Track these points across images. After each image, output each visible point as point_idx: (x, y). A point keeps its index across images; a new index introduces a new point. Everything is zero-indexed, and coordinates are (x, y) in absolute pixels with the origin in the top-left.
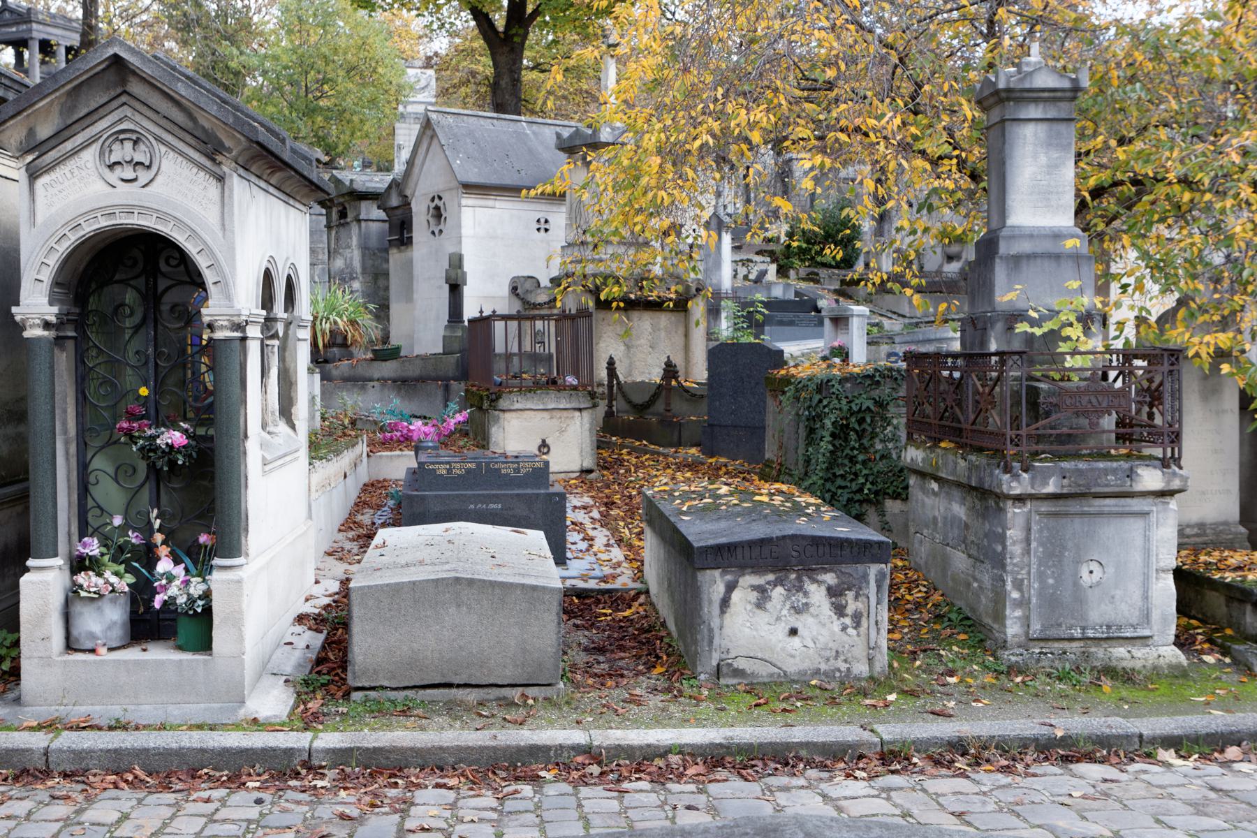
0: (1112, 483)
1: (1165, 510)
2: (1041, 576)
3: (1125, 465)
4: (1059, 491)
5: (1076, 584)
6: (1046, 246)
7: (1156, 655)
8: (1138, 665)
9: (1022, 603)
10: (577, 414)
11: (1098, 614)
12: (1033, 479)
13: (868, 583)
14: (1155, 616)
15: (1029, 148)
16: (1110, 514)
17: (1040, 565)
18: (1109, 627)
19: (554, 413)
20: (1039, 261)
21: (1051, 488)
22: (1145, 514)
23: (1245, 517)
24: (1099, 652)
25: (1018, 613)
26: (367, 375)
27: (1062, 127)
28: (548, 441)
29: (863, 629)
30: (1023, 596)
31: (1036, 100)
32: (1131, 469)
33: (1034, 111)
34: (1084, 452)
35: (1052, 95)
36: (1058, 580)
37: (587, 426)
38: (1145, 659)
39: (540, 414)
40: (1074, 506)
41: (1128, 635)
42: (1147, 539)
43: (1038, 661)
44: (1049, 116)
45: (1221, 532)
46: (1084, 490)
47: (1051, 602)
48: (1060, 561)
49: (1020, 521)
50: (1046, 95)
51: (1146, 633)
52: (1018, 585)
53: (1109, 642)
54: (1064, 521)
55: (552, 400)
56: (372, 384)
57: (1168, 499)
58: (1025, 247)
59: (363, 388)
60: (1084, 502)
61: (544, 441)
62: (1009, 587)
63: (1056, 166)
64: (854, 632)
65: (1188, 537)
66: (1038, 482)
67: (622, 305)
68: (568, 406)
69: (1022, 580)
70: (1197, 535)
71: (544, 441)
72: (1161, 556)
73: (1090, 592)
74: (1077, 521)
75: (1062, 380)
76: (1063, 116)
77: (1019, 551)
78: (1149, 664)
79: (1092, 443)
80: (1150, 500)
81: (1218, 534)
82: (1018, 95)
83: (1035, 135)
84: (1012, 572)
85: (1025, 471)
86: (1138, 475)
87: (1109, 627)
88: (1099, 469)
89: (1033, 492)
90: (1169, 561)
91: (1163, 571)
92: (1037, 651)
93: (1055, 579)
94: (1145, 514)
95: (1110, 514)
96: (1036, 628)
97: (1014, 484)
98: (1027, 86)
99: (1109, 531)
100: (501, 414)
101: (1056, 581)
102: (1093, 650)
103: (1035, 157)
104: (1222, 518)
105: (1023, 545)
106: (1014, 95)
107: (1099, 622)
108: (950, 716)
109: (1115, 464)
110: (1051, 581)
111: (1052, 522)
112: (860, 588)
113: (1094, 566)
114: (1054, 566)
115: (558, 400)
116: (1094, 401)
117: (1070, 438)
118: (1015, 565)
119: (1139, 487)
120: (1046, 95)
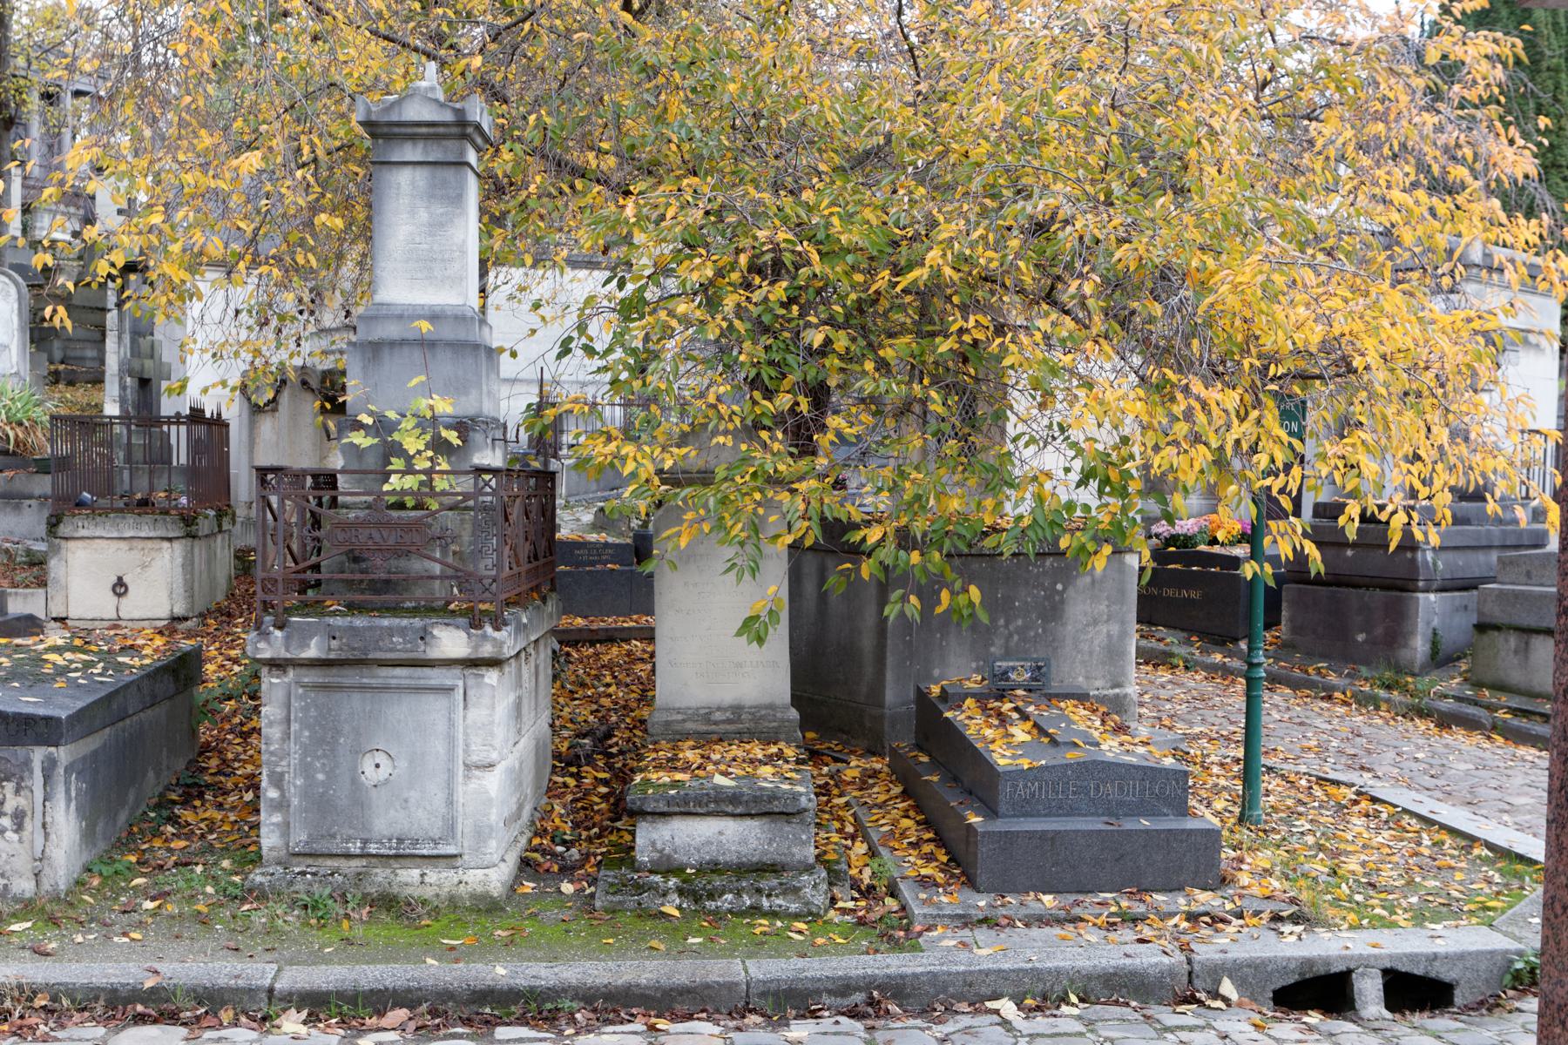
0: (399, 646)
1: (479, 685)
2: (306, 770)
3: (417, 622)
4: (323, 656)
5: (355, 781)
7: (456, 880)
8: (428, 893)
9: (281, 805)
10: (166, 545)
11: (385, 822)
12: (287, 638)
13: (32, 772)
15: (404, 201)
16: (399, 688)
17: (305, 754)
18: (400, 841)
19: (135, 543)
20: (406, 350)
21: (313, 651)
23: (797, 700)
24: (381, 875)
25: (277, 818)
26: (26, 491)
28: (126, 579)
29: (26, 834)
30: (283, 795)
31: (413, 138)
32: (425, 629)
33: (411, 152)
34: (408, 604)
35: (432, 130)
36: (330, 774)
37: (179, 560)
39: (115, 545)
40: (351, 677)
41: (425, 852)
42: (451, 723)
43: (291, 883)
44: (430, 159)
45: (762, 717)
46: (358, 655)
47: (320, 805)
48: (332, 750)
49: (279, 694)
50: (424, 130)
51: (451, 850)
52: (278, 781)
53: (402, 861)
54: (338, 696)
55: (129, 527)
56: (28, 502)
57: (483, 671)
58: (391, 331)
59: (17, 507)
61: (120, 579)
63: (442, 225)
64: (15, 837)
65: (716, 723)
66: (294, 643)
68: (152, 534)
69: (282, 774)
70: (728, 721)
71: (120, 579)
72: (473, 747)
73: (374, 792)
74: (356, 697)
78: (444, 892)
79: (419, 593)
80: (457, 671)
81: (756, 719)
82: (385, 130)
83: (413, 183)
85: (281, 628)
86: (434, 637)
88: (382, 628)
91: (477, 767)
92: (297, 870)
93: (326, 773)
94: (449, 690)
95: (399, 688)
96: (299, 837)
97: (261, 645)
98: (394, 118)
99: (400, 711)
100: (63, 543)
101: (328, 778)
103: (413, 212)
104: (766, 700)
105: (284, 727)
108: (48, 955)
109: (405, 622)
110: (320, 777)
111: (322, 698)
112: (22, 779)
114: (325, 756)
115: (138, 526)
117: (387, 585)
118: (272, 753)
119: (434, 653)
120: (424, 130)
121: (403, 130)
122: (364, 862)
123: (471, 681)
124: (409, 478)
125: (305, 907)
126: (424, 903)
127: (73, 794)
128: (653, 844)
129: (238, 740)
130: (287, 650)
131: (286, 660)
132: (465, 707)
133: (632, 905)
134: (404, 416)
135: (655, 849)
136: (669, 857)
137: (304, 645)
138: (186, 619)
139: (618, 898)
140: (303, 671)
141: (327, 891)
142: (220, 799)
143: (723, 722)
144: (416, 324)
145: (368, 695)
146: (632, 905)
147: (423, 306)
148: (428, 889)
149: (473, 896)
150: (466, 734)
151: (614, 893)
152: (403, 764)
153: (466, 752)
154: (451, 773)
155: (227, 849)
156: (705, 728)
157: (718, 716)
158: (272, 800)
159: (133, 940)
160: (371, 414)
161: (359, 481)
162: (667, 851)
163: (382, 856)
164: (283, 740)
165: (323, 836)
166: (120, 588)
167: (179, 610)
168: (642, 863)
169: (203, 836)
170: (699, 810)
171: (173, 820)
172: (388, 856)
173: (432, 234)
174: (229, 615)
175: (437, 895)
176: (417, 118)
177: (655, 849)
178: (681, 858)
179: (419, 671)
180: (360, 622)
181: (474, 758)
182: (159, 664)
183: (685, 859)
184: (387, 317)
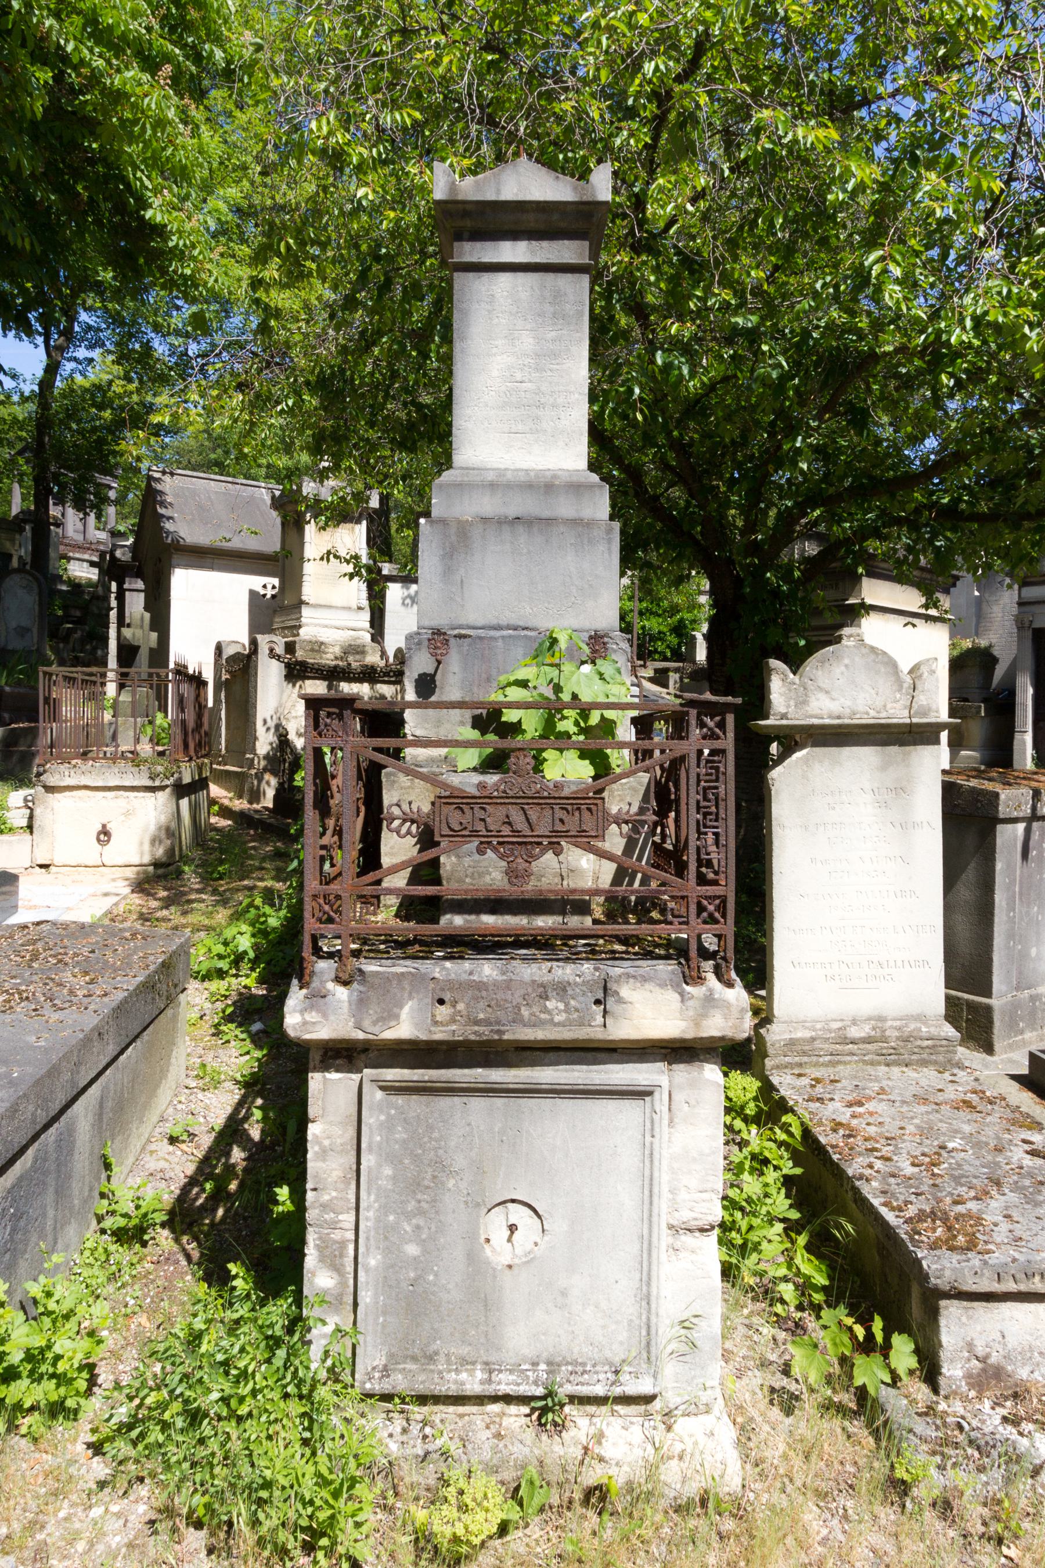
5: (473, 1258)
12: (361, 1004)
17: (385, 1209)
18: (553, 1366)
22: (641, 1094)
27: (563, 281)
28: (108, 827)
51: (645, 1387)
54: (444, 1102)
61: (104, 826)
63: (554, 355)
66: (373, 1011)
71: (104, 826)
75: (200, 784)
86: (621, 1001)
87: (553, 1366)
93: (422, 1243)
94: (641, 1094)
101: (425, 1252)
107: (529, 1352)
110: (412, 1250)
111: (416, 1104)
114: (421, 1212)
116: (518, 818)
128: (970, 1346)
137: (390, 1017)
154: (648, 1247)
157: (854, 1032)
162: (993, 1360)
166: (104, 834)
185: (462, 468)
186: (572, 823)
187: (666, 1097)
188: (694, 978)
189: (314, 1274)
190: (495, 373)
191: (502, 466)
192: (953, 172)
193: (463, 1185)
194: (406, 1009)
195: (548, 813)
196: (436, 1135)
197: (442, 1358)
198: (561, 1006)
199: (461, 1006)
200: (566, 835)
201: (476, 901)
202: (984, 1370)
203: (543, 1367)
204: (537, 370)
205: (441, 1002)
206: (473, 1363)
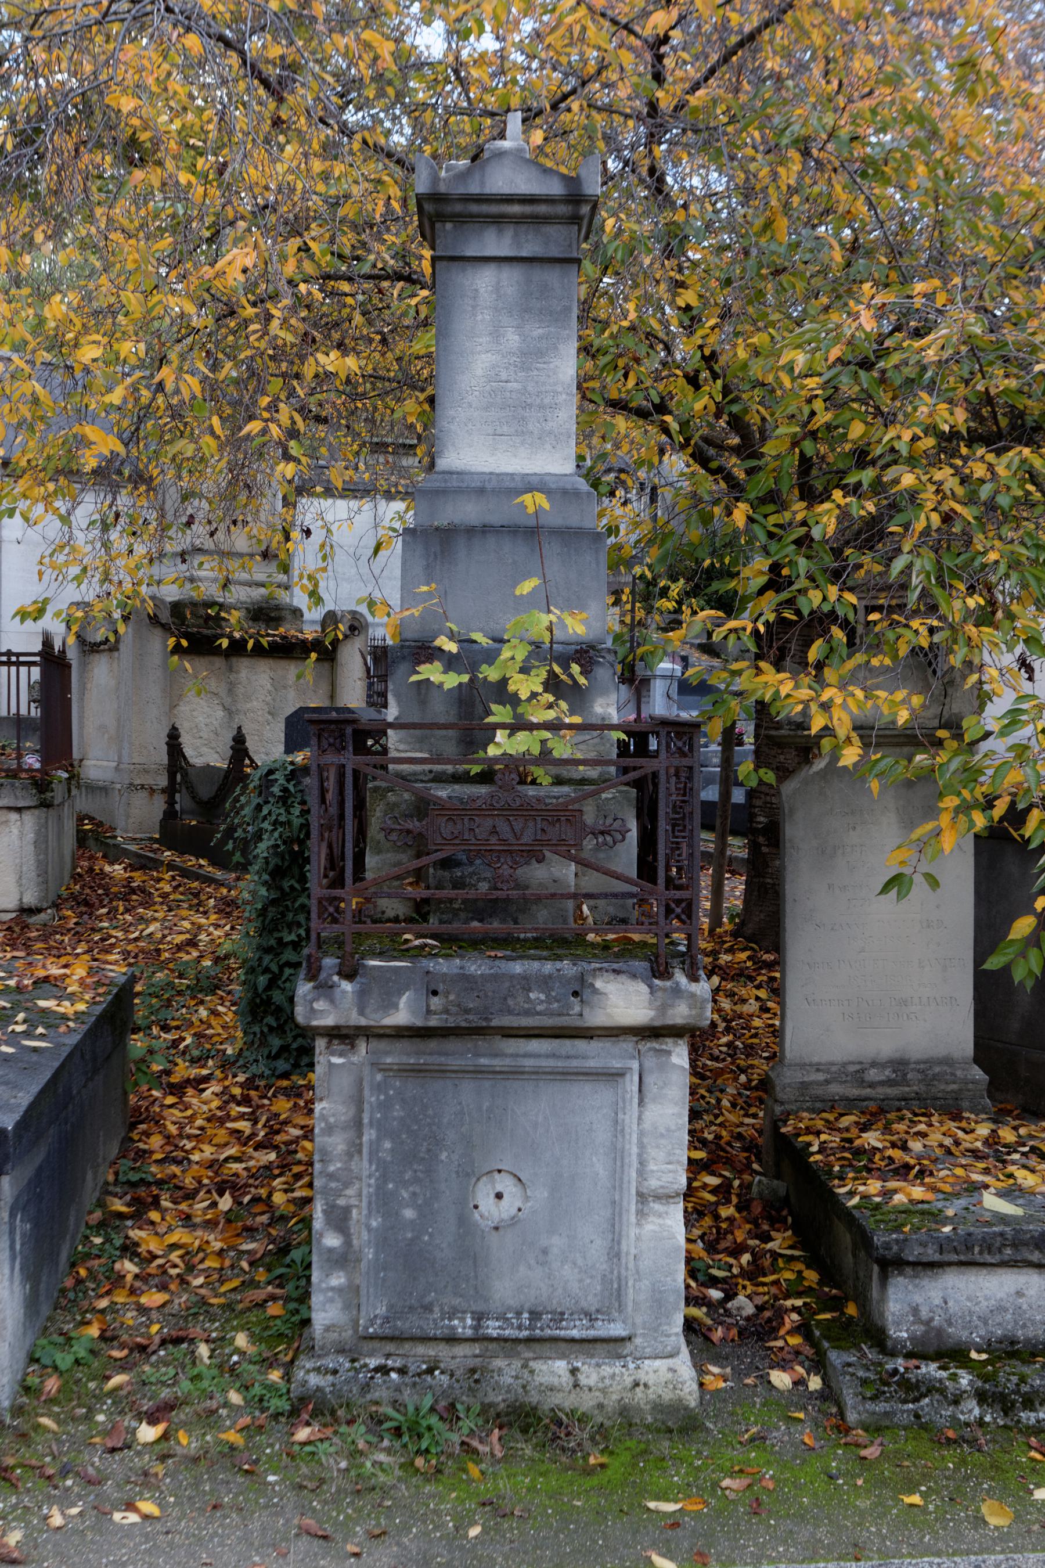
1: (662, 1068)
4: (419, 1023)
5: (463, 1220)
6: (496, 514)
7: (628, 1381)
8: (586, 1402)
9: (342, 1259)
10: (14, 816)
12: (362, 995)
14: (636, 1293)
15: (484, 317)
16: (537, 1073)
18: (535, 1315)
20: (491, 541)
21: (402, 1015)
23: (983, 1053)
25: (338, 1280)
27: (552, 276)
30: (348, 1243)
31: (498, 221)
32: (581, 978)
35: (528, 209)
37: (31, 836)
38: (604, 1391)
41: (575, 1333)
42: (617, 1128)
43: (366, 1388)
44: (524, 254)
45: (935, 1077)
46: (475, 1021)
49: (344, 1083)
50: (516, 209)
51: (617, 1330)
53: (537, 1346)
57: (669, 1044)
60: (482, 1044)
62: (318, 1223)
63: (540, 354)
65: (872, 1085)
66: (373, 1002)
67: (184, 643)
69: (347, 1210)
70: (889, 1083)
72: (652, 1166)
73: (494, 1238)
74: (467, 1087)
76: (555, 252)
77: (341, 1147)
80: (627, 1045)
81: (929, 1081)
82: (458, 208)
83: (497, 289)
84: (325, 1191)
85: (350, 977)
86: (596, 991)
87: (535, 1315)
88: (512, 977)
89: (363, 1022)
90: (667, 1178)
91: (658, 1198)
92: (373, 1363)
93: (419, 1208)
94: (616, 1076)
95: (537, 1073)
97: (320, 1005)
98: (474, 189)
102: (499, 1363)
103: (496, 334)
104: (940, 1052)
105: (351, 1134)
106: (449, 209)
109: (548, 967)
110: (409, 1214)
113: (505, 1184)
114: (416, 1180)
116: (503, 827)
118: (331, 1176)
119: (597, 1018)
120: (516, 209)
121: (485, 208)
122: (477, 1349)
123: (650, 1062)
124: (522, 736)
125: (397, 1432)
126: (583, 1419)
127: (18, 1247)
128: (915, 1311)
129: (170, 1100)
130: (361, 1012)
131: (358, 1028)
132: (641, 1102)
133: (906, 1419)
134: (502, 641)
135: (919, 1320)
136: (940, 1332)
138: (39, 910)
139: (881, 1407)
140: (383, 1045)
141: (428, 1402)
142: (183, 1206)
143: (882, 1083)
144: (519, 500)
145: (487, 1084)
146: (906, 1419)
147: (512, 475)
148: (586, 1396)
149: (658, 1407)
150: (641, 1146)
151: (874, 1398)
152: (540, 1194)
153: (641, 1173)
154: (616, 1208)
155: (229, 1307)
156: (855, 1092)
157: (873, 1075)
158: (331, 1250)
159: (146, 1517)
160: (452, 637)
161: (421, 740)
162: (935, 1323)
163: (506, 1340)
164: (350, 1155)
165: (411, 1308)
167: (30, 899)
168: (897, 1341)
169: (182, 1280)
170: (989, 1259)
171: (129, 1249)
172: (517, 1341)
173: (525, 368)
174: (87, 903)
175: (601, 1406)
176: (506, 190)
177: (919, 1320)
178: (958, 1333)
179: (567, 1046)
180: (476, 966)
181: (653, 1183)
182: (98, 1010)
183: (964, 1335)
184: (459, 491)
185: (444, 472)
186: (553, 833)
187: (636, 1078)
188: (664, 974)
189: (321, 1235)
190: (479, 372)
191: (487, 470)
192: (1000, 102)
193: (455, 1157)
194: (404, 998)
195: (531, 824)
196: (430, 1112)
197: (436, 1309)
198: (542, 997)
199: (452, 997)
200: (548, 843)
201: (444, 1036)
202: (926, 1332)
203: (526, 1315)
204: (522, 369)
205: (435, 993)
206: (464, 1312)
